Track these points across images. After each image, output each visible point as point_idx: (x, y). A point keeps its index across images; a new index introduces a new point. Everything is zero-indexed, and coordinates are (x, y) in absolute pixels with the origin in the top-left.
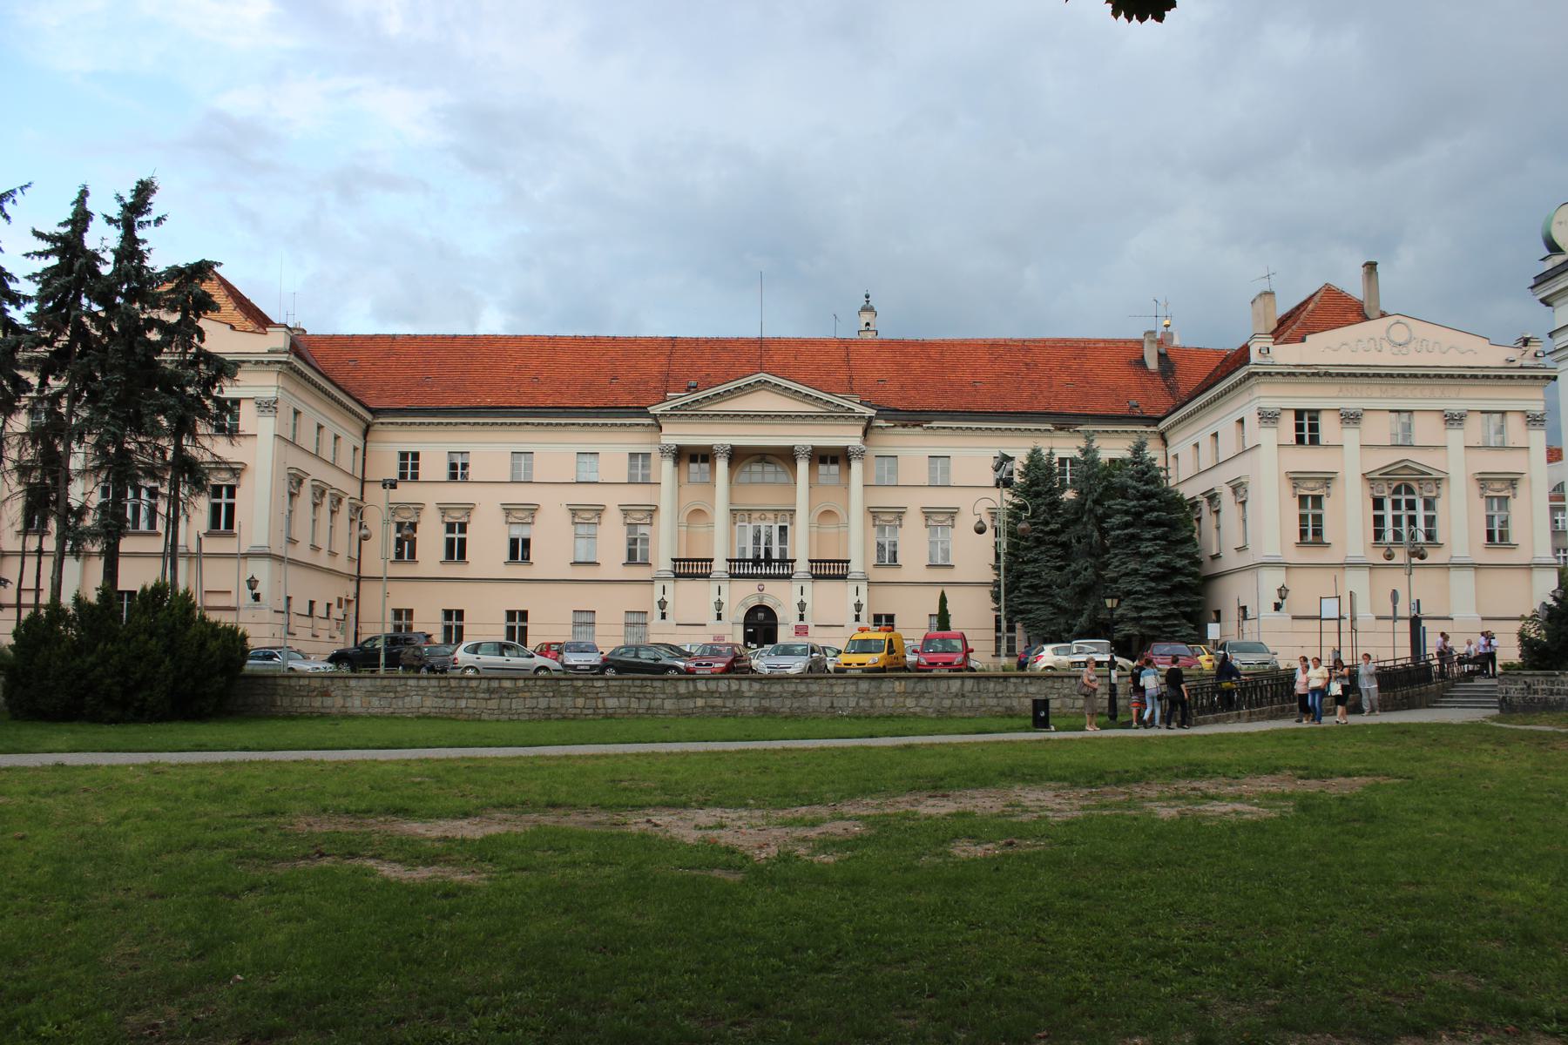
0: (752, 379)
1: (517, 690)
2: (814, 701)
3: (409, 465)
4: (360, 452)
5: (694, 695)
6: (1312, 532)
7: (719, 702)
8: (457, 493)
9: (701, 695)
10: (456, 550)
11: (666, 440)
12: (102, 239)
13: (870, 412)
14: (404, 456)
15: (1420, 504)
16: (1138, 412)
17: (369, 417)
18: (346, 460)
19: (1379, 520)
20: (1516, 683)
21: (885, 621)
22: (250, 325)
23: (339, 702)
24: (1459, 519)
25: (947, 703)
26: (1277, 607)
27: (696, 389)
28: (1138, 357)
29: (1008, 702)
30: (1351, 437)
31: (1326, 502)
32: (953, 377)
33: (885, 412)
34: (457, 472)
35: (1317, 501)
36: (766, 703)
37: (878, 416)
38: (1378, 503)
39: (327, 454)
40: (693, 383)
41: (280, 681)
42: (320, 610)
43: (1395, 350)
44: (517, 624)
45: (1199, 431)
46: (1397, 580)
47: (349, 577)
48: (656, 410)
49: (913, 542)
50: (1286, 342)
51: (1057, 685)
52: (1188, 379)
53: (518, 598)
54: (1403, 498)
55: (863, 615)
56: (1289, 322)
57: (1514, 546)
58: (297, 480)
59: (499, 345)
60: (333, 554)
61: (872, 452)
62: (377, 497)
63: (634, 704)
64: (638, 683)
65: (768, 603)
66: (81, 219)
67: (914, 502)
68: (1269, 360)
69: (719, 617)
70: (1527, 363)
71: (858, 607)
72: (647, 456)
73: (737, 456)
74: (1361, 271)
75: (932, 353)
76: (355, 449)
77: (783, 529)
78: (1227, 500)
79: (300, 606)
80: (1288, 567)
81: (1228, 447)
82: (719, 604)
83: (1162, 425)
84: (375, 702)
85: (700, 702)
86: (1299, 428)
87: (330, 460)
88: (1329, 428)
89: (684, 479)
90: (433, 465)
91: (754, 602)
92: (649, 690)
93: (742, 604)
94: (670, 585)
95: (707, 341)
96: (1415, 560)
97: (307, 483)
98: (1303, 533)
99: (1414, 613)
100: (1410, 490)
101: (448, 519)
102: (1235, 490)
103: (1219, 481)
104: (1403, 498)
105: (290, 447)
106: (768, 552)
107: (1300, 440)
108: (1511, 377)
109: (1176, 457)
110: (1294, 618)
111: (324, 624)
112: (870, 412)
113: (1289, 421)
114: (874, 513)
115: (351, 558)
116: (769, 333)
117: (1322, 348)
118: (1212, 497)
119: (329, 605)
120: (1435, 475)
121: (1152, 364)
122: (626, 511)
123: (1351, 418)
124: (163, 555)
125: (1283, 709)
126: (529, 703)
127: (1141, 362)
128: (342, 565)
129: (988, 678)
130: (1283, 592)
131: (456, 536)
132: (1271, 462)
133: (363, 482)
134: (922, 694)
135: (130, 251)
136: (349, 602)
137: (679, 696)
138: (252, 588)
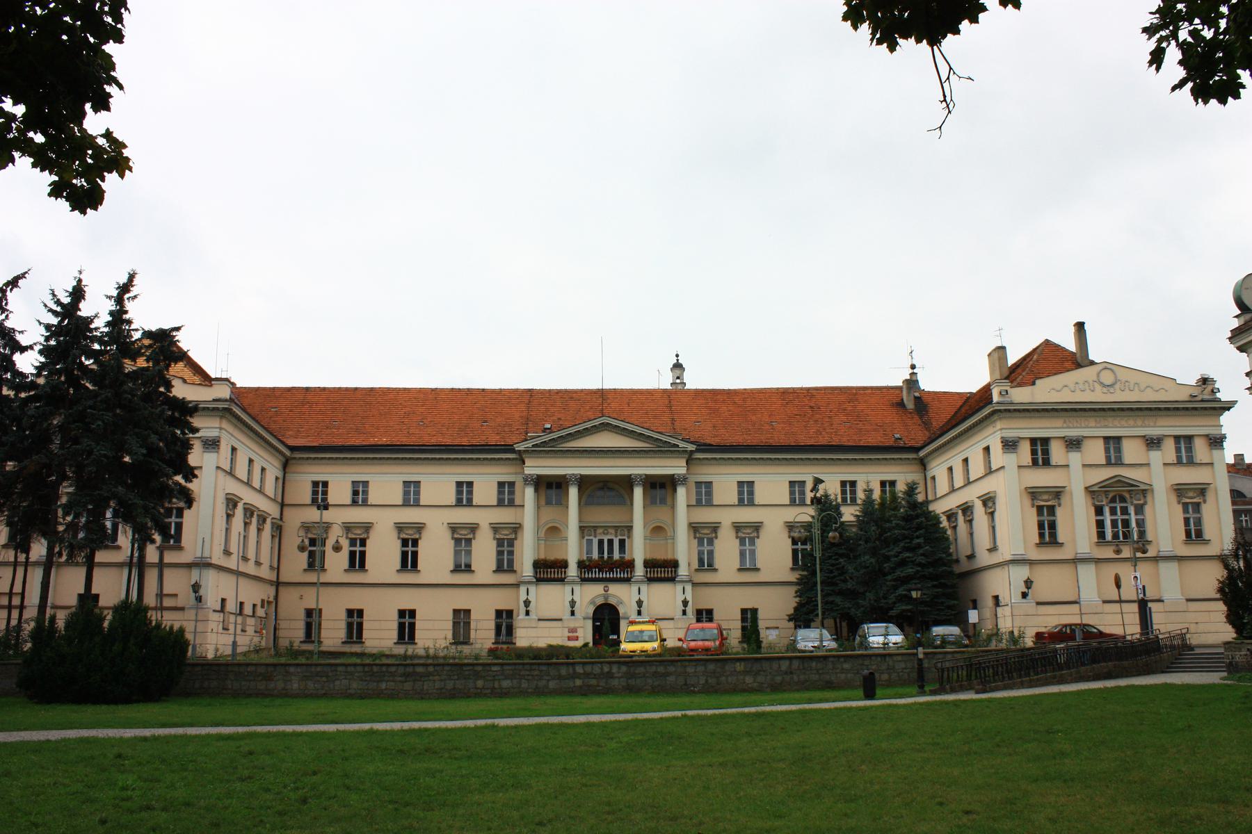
0: (596, 422)
1: (430, 674)
2: (671, 679)
3: (320, 488)
4: (281, 481)
5: (575, 676)
6: (1048, 533)
7: (593, 682)
8: (358, 515)
9: (578, 676)
10: (357, 561)
11: (528, 471)
12: (96, 308)
13: (691, 447)
14: (315, 484)
15: (1132, 510)
16: (901, 444)
17: (288, 453)
18: (270, 488)
19: (1100, 524)
20: (1240, 650)
21: (705, 615)
22: (197, 379)
23: (280, 685)
24: (1163, 523)
25: (778, 679)
26: (1024, 595)
27: (550, 430)
28: (898, 400)
29: (827, 677)
30: (1075, 458)
31: (1059, 511)
32: (754, 418)
33: (704, 447)
34: (359, 494)
35: (1051, 510)
36: (632, 682)
37: (697, 451)
38: (1099, 511)
39: (256, 484)
40: (548, 426)
41: (230, 668)
42: (248, 610)
43: (1105, 390)
44: (407, 620)
45: (954, 458)
46: (1126, 572)
47: (270, 582)
48: (520, 447)
49: (727, 551)
50: (1019, 385)
51: (866, 662)
52: (939, 417)
53: (407, 600)
54: (1118, 506)
55: (689, 609)
56: (1019, 370)
57: (1207, 542)
58: (232, 502)
59: (391, 396)
60: (258, 563)
61: (693, 479)
62: (295, 519)
63: (524, 684)
64: (527, 667)
65: (612, 601)
66: (78, 293)
67: (727, 518)
68: (1007, 399)
69: (573, 613)
70: (1206, 397)
71: (685, 603)
72: (512, 484)
73: (584, 482)
74: (1073, 329)
75: (737, 399)
76: (277, 478)
77: (622, 543)
78: (979, 510)
79: (231, 606)
80: (1031, 563)
81: (977, 469)
82: (573, 603)
83: (922, 454)
84: (311, 685)
85: (578, 682)
86: (1034, 452)
87: (258, 486)
88: (1057, 453)
89: (543, 502)
90: (339, 491)
91: (600, 601)
92: (536, 673)
93: (592, 602)
94: (532, 589)
95: (558, 392)
96: (1139, 555)
97: (240, 506)
98: (1041, 535)
99: (1141, 596)
100: (1123, 500)
101: (351, 536)
102: (985, 503)
103: (971, 495)
104: (1118, 502)
105: (229, 478)
106: (610, 558)
107: (1035, 463)
108: (1195, 409)
109: (933, 478)
110: (1038, 603)
111: (251, 621)
112: (691, 447)
113: (1025, 448)
114: (694, 528)
115: (271, 567)
116: (608, 385)
117: (1047, 390)
118: (967, 509)
119: (254, 606)
120: (1143, 487)
121: (910, 405)
122: (496, 528)
123: (1074, 444)
124: (130, 565)
125: (1054, 677)
126: (438, 685)
127: (901, 404)
128: (265, 572)
129: (811, 658)
130: (1028, 583)
131: (358, 549)
132: (1009, 481)
133: (283, 505)
134: (757, 673)
135: (118, 318)
136: (269, 603)
137: (560, 677)
138: (195, 592)
